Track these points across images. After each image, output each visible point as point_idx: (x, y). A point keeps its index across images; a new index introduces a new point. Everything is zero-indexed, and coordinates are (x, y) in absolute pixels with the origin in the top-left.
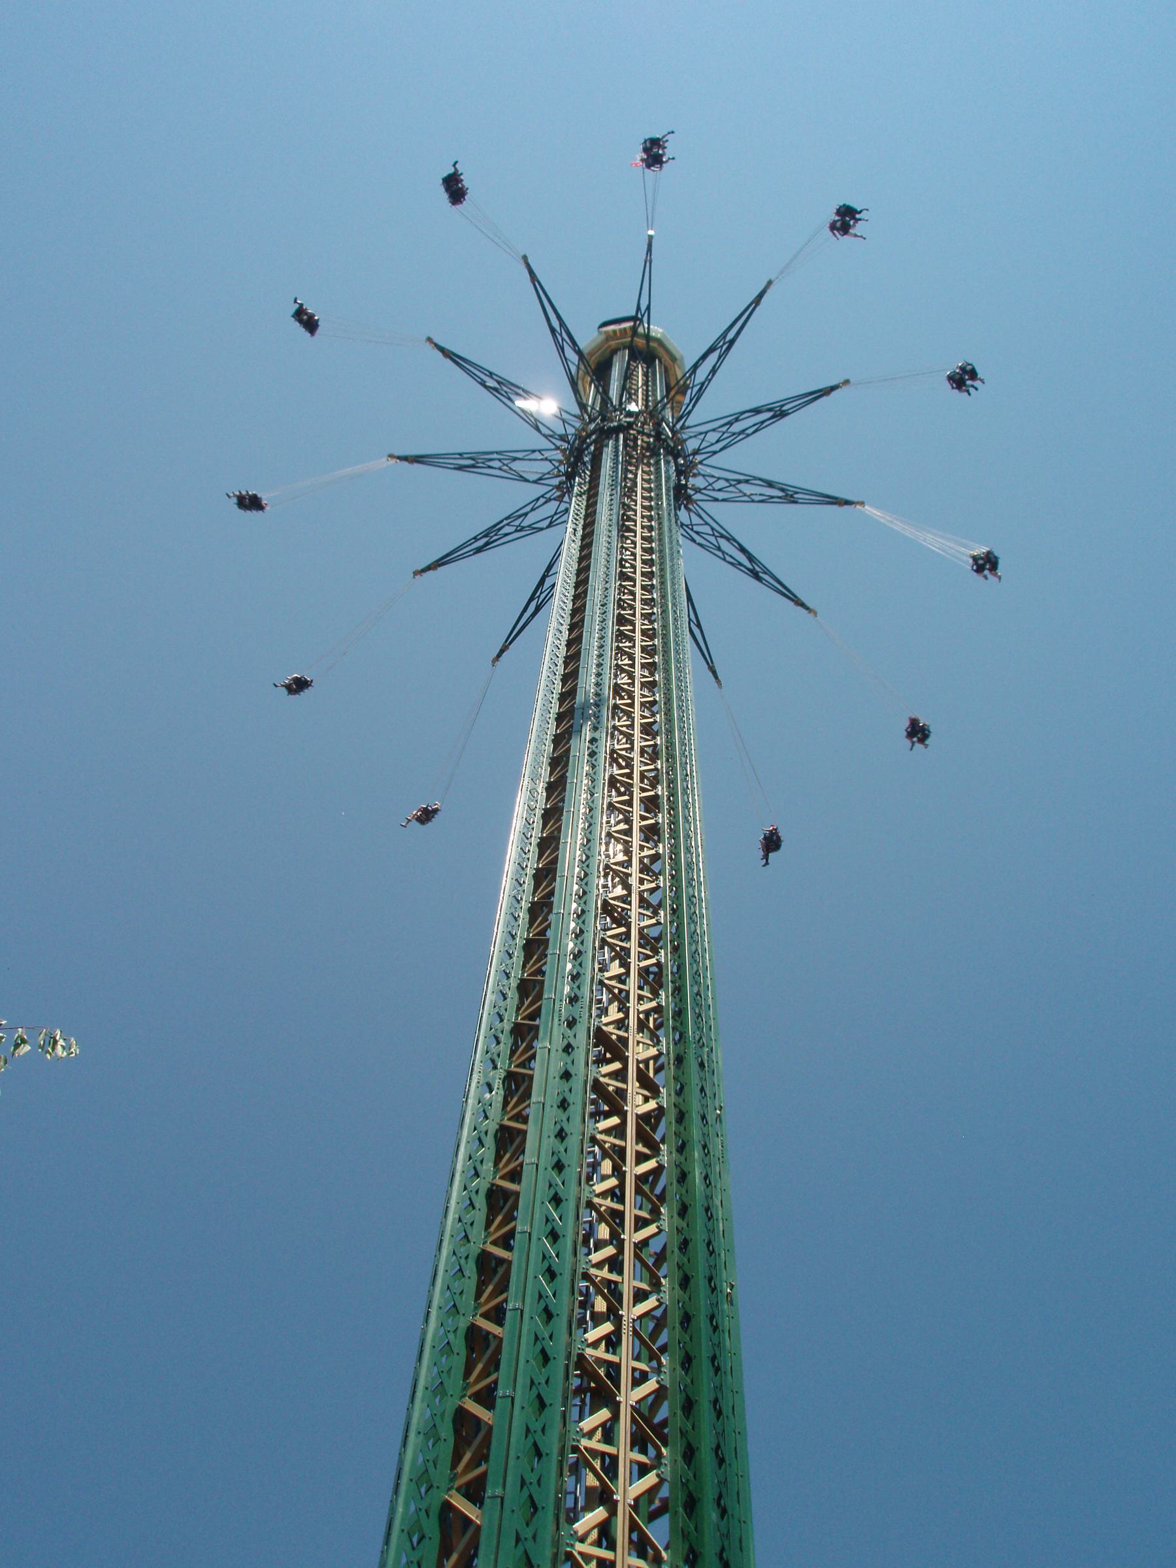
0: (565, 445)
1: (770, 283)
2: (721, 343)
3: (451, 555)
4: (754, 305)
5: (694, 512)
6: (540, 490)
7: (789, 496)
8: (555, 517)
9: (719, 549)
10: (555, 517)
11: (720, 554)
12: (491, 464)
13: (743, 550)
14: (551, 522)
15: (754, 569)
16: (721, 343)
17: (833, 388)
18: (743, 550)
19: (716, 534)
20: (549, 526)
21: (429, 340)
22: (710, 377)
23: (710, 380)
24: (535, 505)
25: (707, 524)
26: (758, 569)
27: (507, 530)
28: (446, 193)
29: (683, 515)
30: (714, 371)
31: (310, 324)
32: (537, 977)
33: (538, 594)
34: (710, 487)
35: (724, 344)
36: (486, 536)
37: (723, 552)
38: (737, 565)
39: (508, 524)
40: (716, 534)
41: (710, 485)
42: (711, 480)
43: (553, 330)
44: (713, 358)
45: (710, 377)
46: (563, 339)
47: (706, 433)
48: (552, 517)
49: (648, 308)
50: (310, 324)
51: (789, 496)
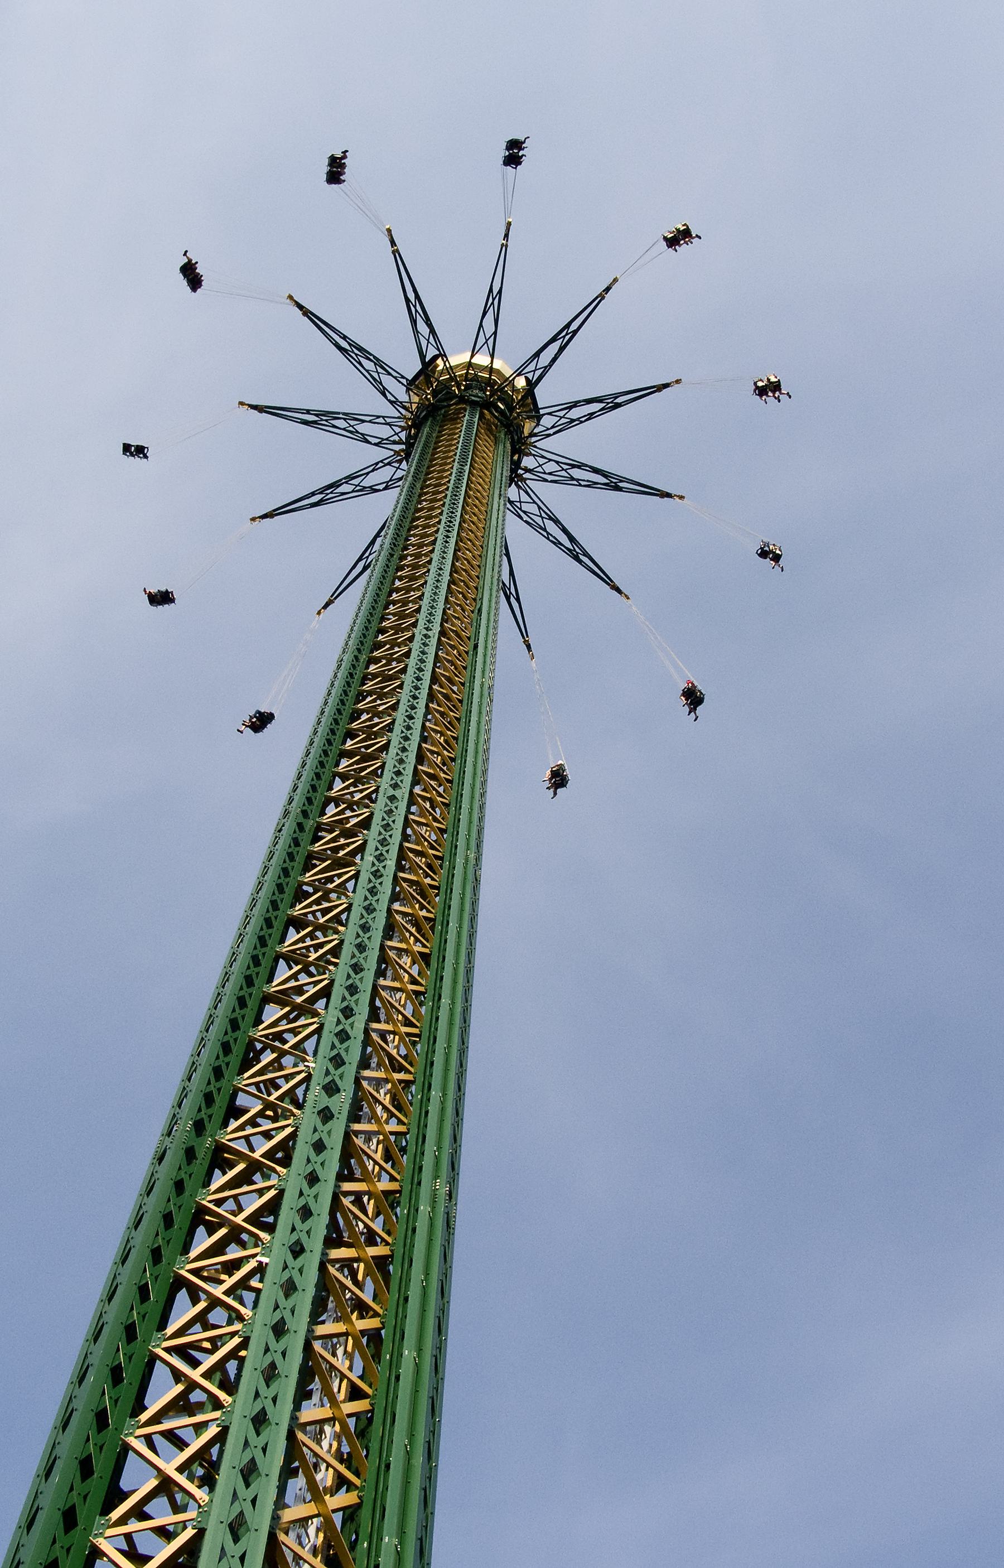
0: (409, 415)
1: (615, 280)
2: (609, 401)
3: (284, 411)
4: (599, 299)
5: (523, 490)
6: (382, 454)
7: (614, 484)
8: (385, 442)
9: (545, 530)
10: (385, 442)
11: (545, 534)
12: (334, 422)
13: (565, 530)
14: (380, 443)
15: (575, 550)
16: (609, 401)
17: (666, 386)
18: (565, 530)
19: (544, 515)
20: (376, 444)
21: (291, 297)
22: (583, 419)
23: (582, 422)
24: (374, 419)
25: (534, 502)
26: (578, 550)
27: (345, 488)
28: (326, 175)
29: (513, 492)
30: (591, 416)
31: (140, 451)
32: (321, 904)
33: (367, 554)
34: (539, 469)
35: (612, 402)
36: (321, 493)
37: (548, 533)
38: (592, 485)
39: (346, 483)
40: (544, 515)
41: (540, 466)
42: (542, 461)
43: (407, 300)
44: (596, 407)
45: (583, 419)
46: (416, 311)
47: (550, 460)
48: (383, 439)
49: (500, 292)
50: (140, 451)
51: (614, 484)
